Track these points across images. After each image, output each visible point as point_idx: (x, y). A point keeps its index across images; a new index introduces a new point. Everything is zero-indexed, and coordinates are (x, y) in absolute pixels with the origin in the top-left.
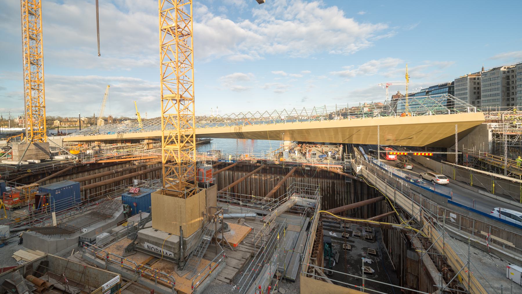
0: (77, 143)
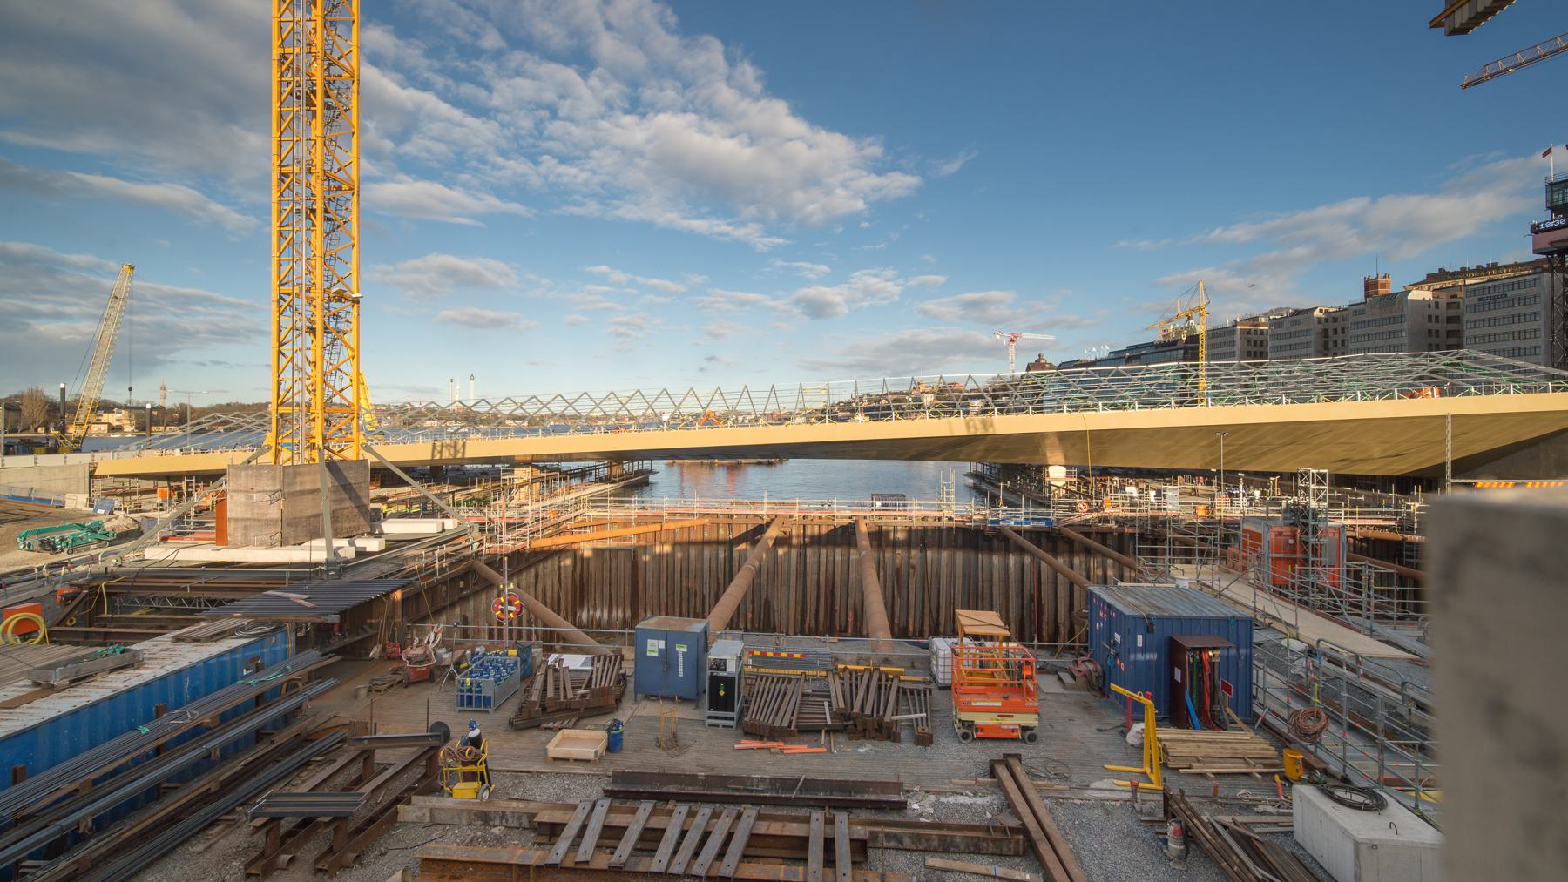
0: (149, 484)
